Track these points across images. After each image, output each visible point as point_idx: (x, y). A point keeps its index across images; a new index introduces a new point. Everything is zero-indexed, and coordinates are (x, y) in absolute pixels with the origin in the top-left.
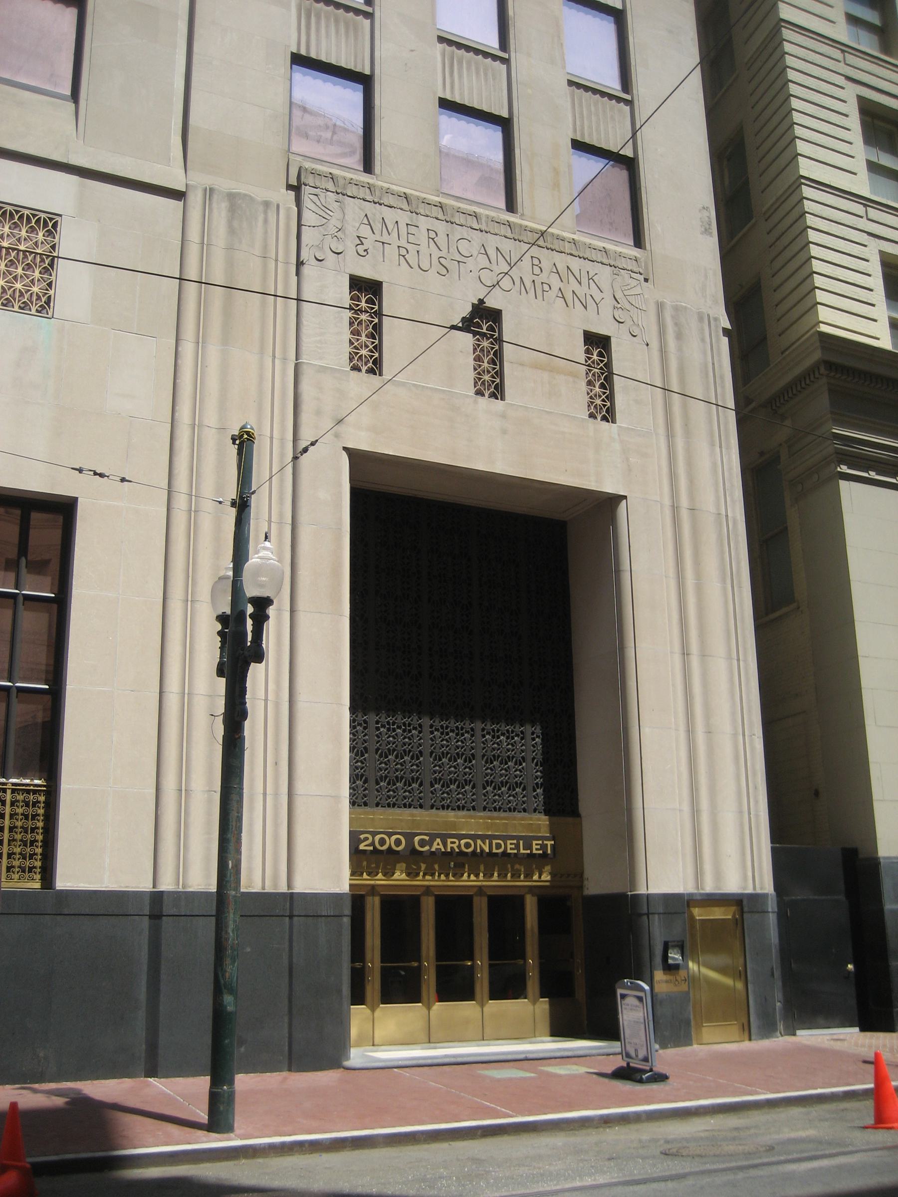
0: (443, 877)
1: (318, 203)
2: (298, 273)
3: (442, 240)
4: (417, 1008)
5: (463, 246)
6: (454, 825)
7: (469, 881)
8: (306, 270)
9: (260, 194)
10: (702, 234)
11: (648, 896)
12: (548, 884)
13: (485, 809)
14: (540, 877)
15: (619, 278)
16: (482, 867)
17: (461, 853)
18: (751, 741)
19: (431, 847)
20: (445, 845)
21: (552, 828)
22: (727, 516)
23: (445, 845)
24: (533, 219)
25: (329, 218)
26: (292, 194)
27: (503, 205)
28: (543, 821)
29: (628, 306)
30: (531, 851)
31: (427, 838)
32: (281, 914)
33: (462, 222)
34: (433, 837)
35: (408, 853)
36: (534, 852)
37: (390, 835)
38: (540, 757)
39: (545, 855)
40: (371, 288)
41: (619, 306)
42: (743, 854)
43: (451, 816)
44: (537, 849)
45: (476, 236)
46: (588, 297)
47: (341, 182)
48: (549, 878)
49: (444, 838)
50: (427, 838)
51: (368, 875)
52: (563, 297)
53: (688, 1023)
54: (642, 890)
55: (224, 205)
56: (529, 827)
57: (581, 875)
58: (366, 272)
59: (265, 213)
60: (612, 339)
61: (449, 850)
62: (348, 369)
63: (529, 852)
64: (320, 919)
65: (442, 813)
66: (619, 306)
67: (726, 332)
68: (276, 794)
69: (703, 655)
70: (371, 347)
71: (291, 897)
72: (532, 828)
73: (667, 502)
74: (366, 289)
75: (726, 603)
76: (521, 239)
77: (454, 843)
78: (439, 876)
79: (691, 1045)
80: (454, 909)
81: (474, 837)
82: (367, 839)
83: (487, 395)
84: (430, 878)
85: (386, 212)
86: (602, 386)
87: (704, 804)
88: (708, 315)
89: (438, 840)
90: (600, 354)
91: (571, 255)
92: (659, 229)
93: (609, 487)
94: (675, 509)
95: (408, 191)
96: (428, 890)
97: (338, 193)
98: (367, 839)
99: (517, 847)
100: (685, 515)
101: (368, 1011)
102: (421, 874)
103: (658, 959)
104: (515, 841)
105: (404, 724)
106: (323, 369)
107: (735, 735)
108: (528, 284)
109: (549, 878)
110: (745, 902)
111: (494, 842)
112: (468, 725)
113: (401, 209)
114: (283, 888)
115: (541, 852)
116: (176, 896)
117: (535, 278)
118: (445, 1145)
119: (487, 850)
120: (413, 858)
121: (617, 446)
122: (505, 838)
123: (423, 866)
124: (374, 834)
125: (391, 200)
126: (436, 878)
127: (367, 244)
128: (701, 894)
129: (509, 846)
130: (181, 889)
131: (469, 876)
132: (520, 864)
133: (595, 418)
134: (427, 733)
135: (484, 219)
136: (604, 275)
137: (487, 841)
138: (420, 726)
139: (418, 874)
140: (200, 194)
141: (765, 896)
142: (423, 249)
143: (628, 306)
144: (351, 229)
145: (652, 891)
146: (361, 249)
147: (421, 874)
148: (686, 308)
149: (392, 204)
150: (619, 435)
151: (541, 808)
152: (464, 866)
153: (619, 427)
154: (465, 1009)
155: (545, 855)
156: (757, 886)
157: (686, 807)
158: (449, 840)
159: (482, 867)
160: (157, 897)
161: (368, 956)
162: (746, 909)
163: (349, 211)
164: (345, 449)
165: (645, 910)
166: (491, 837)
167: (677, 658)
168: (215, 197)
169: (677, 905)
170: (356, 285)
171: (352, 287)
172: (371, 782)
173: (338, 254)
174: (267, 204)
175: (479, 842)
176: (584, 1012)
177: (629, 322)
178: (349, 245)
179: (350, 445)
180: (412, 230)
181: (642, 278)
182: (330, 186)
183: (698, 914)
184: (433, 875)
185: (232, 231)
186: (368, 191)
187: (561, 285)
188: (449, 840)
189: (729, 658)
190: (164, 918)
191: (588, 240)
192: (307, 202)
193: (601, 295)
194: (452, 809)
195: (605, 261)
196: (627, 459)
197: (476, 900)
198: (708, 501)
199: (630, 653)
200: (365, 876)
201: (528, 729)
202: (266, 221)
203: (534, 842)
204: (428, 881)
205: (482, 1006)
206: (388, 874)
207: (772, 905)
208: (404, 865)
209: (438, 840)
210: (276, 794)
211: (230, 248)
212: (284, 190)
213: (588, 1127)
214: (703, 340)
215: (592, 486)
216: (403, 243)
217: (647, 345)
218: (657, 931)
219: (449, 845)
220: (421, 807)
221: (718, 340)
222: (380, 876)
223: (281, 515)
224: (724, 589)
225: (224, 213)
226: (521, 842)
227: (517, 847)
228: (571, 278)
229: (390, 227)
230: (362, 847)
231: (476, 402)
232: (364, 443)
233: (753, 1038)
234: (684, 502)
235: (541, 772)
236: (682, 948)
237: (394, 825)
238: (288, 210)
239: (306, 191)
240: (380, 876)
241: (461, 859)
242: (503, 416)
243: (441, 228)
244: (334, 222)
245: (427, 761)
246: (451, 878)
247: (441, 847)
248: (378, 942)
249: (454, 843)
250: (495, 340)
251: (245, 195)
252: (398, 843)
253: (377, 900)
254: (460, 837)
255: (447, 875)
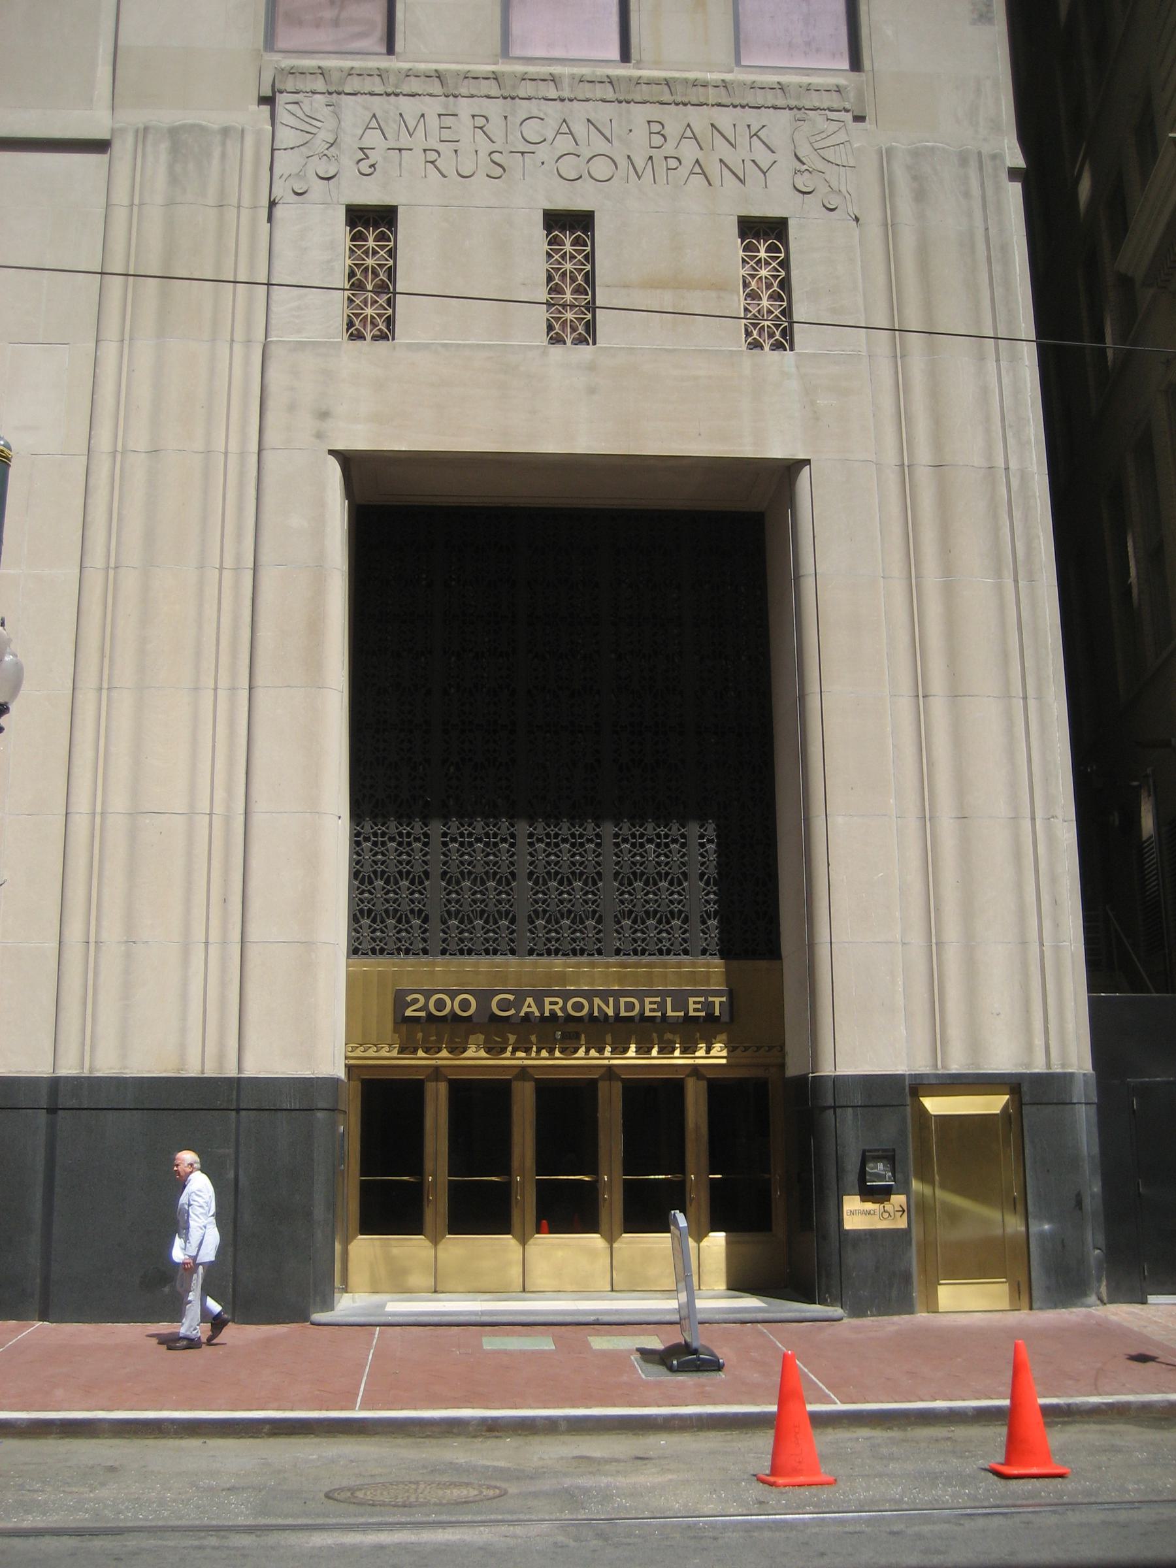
0: (544, 1053)
1: (300, 114)
2: (270, 219)
3: (495, 127)
4: (595, 1240)
5: (532, 130)
6: (562, 978)
7: (584, 1058)
8: (279, 211)
9: (214, 119)
10: (974, 23)
11: (836, 1079)
12: (724, 1061)
13: (618, 952)
14: (708, 1051)
15: (805, 127)
16: (609, 1038)
17: (569, 1018)
18: (1049, 829)
19: (519, 1010)
20: (541, 1007)
21: (729, 976)
22: (1007, 469)
23: (541, 1007)
24: (657, 64)
25: (313, 130)
26: (266, 109)
27: (846, 65)
28: (716, 966)
29: (821, 165)
30: (687, 1014)
31: (511, 997)
32: (224, 1106)
33: (531, 93)
34: (521, 996)
35: (486, 1020)
36: (692, 1013)
37: (453, 994)
38: (712, 872)
39: (710, 1017)
40: (383, 219)
41: (805, 167)
42: (1027, 1009)
43: (558, 964)
44: (696, 1010)
45: (553, 111)
46: (749, 164)
47: (335, 76)
48: (724, 1053)
49: (539, 997)
50: (511, 997)
51: (561, 1052)
52: (704, 173)
53: (907, 1278)
54: (827, 1069)
55: (164, 146)
56: (692, 977)
57: (782, 1048)
58: (371, 195)
59: (224, 144)
60: (790, 222)
61: (547, 1014)
62: (546, 342)
63: (682, 1014)
64: (279, 1113)
65: (545, 960)
66: (805, 167)
67: (1014, 174)
68: (224, 942)
69: (955, 695)
70: (776, 313)
71: (237, 1084)
72: (702, 977)
73: (891, 458)
74: (372, 221)
75: (1002, 608)
76: (629, 98)
77: (556, 1003)
78: (538, 1051)
79: (910, 1311)
80: (567, 1102)
81: (589, 995)
82: (416, 1001)
83: (369, 337)
84: (523, 1055)
85: (405, 103)
86: (578, 290)
87: (952, 932)
88: (980, 154)
89: (530, 1000)
90: (382, 237)
91: (719, 105)
92: (889, 33)
93: (777, 450)
94: (906, 469)
95: (441, 67)
96: (523, 1072)
97: (330, 93)
98: (416, 1001)
99: (662, 1006)
100: (924, 478)
101: (427, 1243)
102: (510, 1049)
103: (852, 1178)
104: (658, 999)
105: (401, 835)
106: (301, 346)
107: (1015, 819)
108: (640, 163)
109: (724, 1053)
110: (1024, 1089)
111: (623, 1000)
112: (418, 828)
113: (431, 95)
114: (231, 1072)
115: (703, 1014)
116: (76, 1083)
117: (653, 152)
118: (194, 1443)
119: (610, 1012)
120: (496, 1028)
121: (794, 385)
122: (640, 995)
123: (512, 1038)
124: (428, 994)
125: (414, 85)
126: (533, 1054)
127: (374, 156)
128: (937, 1076)
129: (648, 1007)
130: (86, 1073)
131: (587, 1052)
132: (674, 1033)
133: (762, 348)
134: (438, 842)
135: (566, 82)
136: (778, 125)
137: (611, 1000)
138: (513, 836)
139: (504, 1050)
140: (130, 139)
141: (1067, 1078)
142: (465, 145)
143: (821, 165)
144: (349, 141)
145: (842, 1071)
146: (364, 167)
147: (510, 1049)
148: (933, 149)
149: (414, 90)
150: (797, 367)
151: (714, 948)
152: (578, 1037)
153: (798, 354)
154: (411, 1248)
155: (710, 1017)
156: (87, 1066)
157: (917, 938)
158: (547, 1000)
159: (609, 1038)
160: (55, 1083)
161: (429, 1165)
162: (1026, 1099)
163: (348, 119)
164: (332, 452)
165: (830, 1102)
166: (617, 994)
167: (905, 704)
168: (150, 137)
169: (895, 1094)
170: (750, 229)
171: (743, 235)
172: (380, 920)
173: (328, 179)
174: (225, 132)
175: (597, 1001)
176: (791, 1259)
177: (823, 189)
178: (347, 163)
179: (340, 446)
180: (448, 121)
181: (848, 117)
182: (320, 85)
183: (934, 1105)
184: (528, 1050)
185: (174, 179)
186: (377, 79)
187: (700, 155)
188: (547, 1000)
189: (1007, 695)
190: (60, 1112)
191: (347, 63)
192: (283, 115)
193: (771, 157)
194: (563, 955)
195: (781, 102)
196: (813, 403)
197: (517, 1086)
198: (969, 449)
199: (813, 702)
200: (421, 1053)
201: (693, 829)
202: (223, 155)
203: (691, 1000)
204: (521, 1059)
205: (523, 1242)
206: (457, 1049)
207: (1084, 1093)
208: (482, 1037)
209: (530, 1000)
210: (224, 942)
211: (170, 203)
212: (254, 107)
213: (459, 1435)
214: (967, 195)
215: (746, 449)
216: (433, 143)
217: (857, 219)
218: (849, 1135)
219: (547, 1007)
220: (513, 952)
221: (998, 188)
222: (444, 1053)
223: (238, 557)
224: (999, 588)
225: (164, 157)
226: (669, 1000)
227: (662, 1006)
228: (719, 140)
229: (411, 124)
230: (408, 1013)
231: (544, 353)
232: (361, 440)
233: (1034, 1306)
234: (924, 455)
235: (715, 893)
236: (890, 1158)
237: (447, 979)
238: (258, 133)
239: (281, 99)
240: (444, 1053)
241: (571, 1027)
242: (592, 367)
243: (494, 109)
244: (325, 135)
245: (523, 887)
246: (557, 1054)
247: (534, 1009)
248: (444, 1146)
249: (556, 1003)
250: (780, 264)
251: (193, 126)
252: (465, 1005)
253: (443, 1087)
254: (566, 995)
255: (551, 1051)
